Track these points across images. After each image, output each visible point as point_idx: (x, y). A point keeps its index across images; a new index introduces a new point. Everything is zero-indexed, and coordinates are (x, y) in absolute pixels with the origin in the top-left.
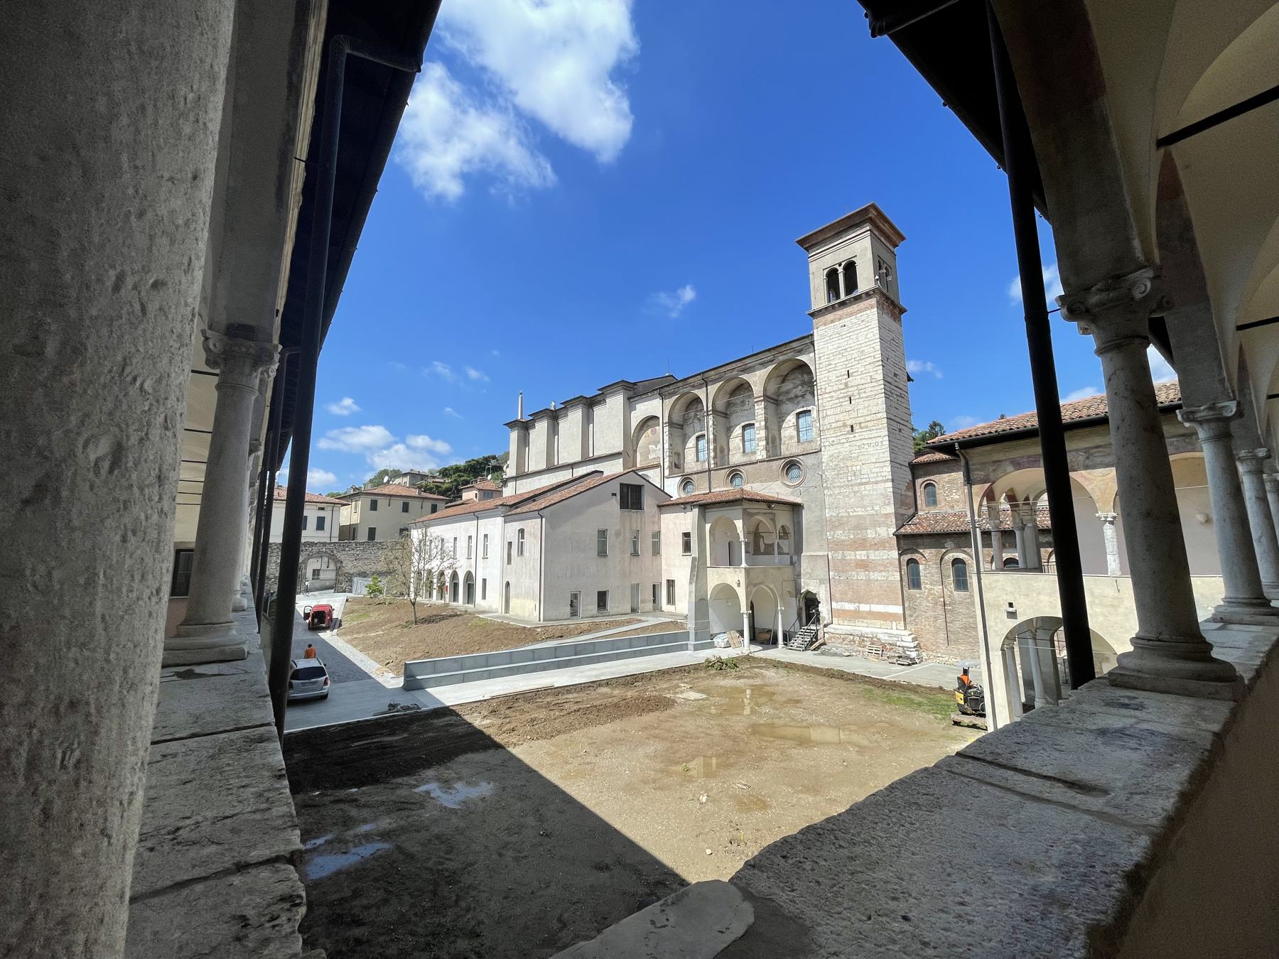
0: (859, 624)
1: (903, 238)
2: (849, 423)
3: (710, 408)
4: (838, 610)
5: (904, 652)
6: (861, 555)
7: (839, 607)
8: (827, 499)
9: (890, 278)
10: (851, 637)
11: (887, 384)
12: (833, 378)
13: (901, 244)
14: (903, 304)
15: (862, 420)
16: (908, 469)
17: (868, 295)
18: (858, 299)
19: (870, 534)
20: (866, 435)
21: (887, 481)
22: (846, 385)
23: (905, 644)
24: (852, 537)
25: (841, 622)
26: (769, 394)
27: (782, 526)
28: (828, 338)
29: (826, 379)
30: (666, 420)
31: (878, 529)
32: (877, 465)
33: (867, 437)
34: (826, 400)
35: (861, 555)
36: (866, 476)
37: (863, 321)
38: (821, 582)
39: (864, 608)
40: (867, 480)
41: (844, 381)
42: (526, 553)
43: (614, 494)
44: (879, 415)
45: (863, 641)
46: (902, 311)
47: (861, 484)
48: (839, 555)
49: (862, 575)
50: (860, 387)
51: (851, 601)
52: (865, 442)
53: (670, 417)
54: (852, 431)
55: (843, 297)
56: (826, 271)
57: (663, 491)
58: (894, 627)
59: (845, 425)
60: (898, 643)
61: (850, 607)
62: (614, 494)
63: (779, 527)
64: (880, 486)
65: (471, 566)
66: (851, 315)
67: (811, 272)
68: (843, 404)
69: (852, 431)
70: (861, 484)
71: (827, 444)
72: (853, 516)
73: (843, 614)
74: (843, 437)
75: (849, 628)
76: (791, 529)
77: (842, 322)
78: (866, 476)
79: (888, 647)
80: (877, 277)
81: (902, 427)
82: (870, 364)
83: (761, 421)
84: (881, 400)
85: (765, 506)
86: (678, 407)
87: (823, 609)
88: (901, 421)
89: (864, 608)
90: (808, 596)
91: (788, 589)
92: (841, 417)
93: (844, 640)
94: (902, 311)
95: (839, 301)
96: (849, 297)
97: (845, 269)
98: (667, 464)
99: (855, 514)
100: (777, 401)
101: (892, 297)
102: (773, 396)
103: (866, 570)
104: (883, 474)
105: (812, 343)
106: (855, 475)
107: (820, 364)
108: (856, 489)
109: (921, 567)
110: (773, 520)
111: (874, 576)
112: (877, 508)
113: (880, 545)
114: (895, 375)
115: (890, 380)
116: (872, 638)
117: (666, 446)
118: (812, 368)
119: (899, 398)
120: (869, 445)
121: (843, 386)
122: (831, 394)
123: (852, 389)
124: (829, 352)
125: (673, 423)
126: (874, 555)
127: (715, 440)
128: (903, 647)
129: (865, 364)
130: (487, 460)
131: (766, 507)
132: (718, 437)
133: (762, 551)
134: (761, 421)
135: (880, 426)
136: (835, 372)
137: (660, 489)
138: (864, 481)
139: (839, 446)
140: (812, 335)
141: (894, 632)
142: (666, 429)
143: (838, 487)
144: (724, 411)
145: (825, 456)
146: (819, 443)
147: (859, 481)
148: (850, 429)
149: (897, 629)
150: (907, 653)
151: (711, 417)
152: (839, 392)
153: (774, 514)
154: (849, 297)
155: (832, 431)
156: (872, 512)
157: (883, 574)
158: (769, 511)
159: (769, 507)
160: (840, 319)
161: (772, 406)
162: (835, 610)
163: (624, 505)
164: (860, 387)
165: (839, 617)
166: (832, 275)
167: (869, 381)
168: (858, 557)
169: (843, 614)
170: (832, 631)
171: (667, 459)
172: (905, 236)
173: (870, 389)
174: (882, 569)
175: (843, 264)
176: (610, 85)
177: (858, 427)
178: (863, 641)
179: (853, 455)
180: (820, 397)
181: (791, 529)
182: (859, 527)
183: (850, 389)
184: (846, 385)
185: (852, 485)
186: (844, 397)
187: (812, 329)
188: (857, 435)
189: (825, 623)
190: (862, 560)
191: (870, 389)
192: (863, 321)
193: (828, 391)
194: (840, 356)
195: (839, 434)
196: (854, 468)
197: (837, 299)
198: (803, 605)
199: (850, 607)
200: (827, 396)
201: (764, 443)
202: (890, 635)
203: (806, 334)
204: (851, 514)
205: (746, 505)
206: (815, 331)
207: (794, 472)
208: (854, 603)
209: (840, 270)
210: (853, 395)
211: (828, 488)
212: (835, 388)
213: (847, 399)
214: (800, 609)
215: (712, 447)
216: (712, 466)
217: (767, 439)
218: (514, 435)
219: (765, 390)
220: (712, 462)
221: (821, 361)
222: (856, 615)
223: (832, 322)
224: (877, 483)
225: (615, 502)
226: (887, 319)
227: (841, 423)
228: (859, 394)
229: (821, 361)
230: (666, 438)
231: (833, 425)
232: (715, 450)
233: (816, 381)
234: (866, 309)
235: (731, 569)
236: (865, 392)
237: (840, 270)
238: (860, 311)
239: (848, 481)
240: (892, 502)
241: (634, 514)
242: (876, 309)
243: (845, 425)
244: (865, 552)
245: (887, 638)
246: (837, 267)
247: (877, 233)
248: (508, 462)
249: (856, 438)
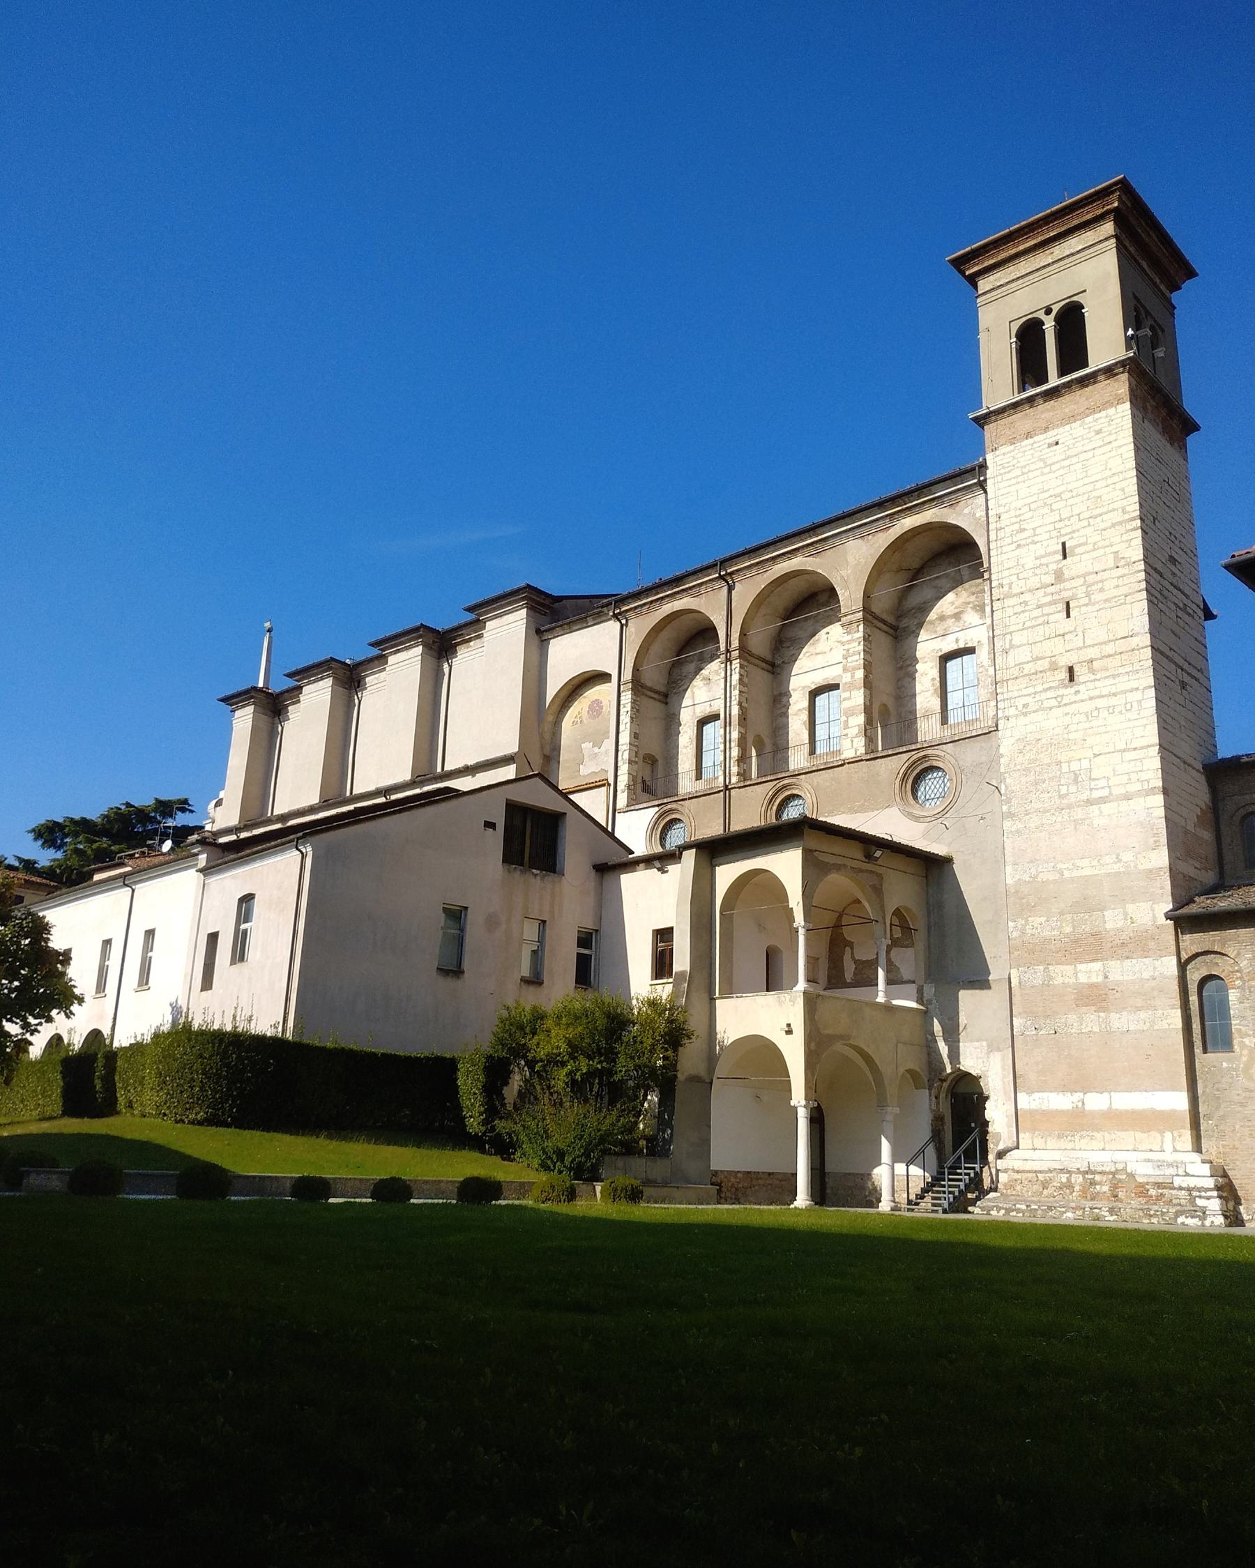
0: (1083, 1143)
1: (1191, 274)
2: (1065, 661)
3: (735, 643)
4: (1032, 1113)
5: (1192, 1200)
6: (1089, 972)
7: (1034, 1106)
8: (1008, 843)
9: (1160, 353)
10: (1064, 1178)
11: (1152, 572)
12: (1029, 562)
13: (1188, 285)
14: (1191, 405)
15: (1092, 653)
16: (1202, 779)
17: (1109, 371)
18: (1084, 382)
19: (1113, 920)
20: (1106, 686)
21: (1151, 791)
22: (1059, 576)
23: (1192, 1182)
24: (1068, 929)
25: (1039, 1143)
26: (876, 608)
27: (897, 913)
28: (1018, 472)
29: (1012, 563)
30: (627, 675)
31: (1130, 908)
32: (1129, 756)
33: (1105, 691)
34: (1010, 611)
35: (1089, 972)
36: (1102, 783)
37: (1098, 432)
38: (993, 1048)
39: (1096, 1102)
40: (1105, 793)
41: (1054, 566)
42: (254, 950)
43: (490, 825)
44: (1135, 641)
45: (1093, 1183)
46: (1190, 426)
47: (1090, 802)
48: (1036, 975)
49: (1091, 1021)
50: (1090, 579)
51: (1066, 1088)
52: (1101, 703)
53: (636, 669)
54: (1071, 679)
55: (1054, 380)
56: (1016, 327)
57: (611, 835)
58: (1168, 1146)
59: (1054, 667)
60: (1178, 1182)
61: (1061, 1102)
62: (490, 825)
63: (890, 910)
64: (1139, 804)
65: (101, 1017)
66: (1072, 418)
67: (982, 326)
68: (1052, 618)
69: (1071, 679)
70: (1090, 802)
71: (1012, 711)
72: (1072, 880)
73: (1047, 1122)
74: (1050, 694)
75: (1057, 1155)
76: (918, 922)
77: (1052, 435)
78: (1102, 783)
79: (1153, 1192)
80: (1130, 332)
81: (1187, 679)
82: (1113, 525)
83: (855, 669)
84: (1140, 606)
85: (855, 851)
86: (656, 648)
87: (997, 1114)
88: (1186, 666)
89: (1096, 1102)
90: (961, 1089)
91: (911, 1066)
92: (1047, 648)
93: (1045, 1185)
94: (1190, 426)
95: (1044, 387)
96: (1067, 379)
97: (1059, 319)
98: (623, 780)
99: (1076, 874)
100: (895, 628)
101: (1163, 381)
102: (884, 616)
103: (1105, 1010)
104: (1144, 776)
105: (982, 485)
106: (1076, 781)
107: (997, 530)
108: (1079, 813)
109: (1233, 995)
110: (878, 891)
111: (1121, 1021)
112: (1127, 857)
113: (1133, 945)
114: (1173, 560)
115: (1159, 566)
116: (1114, 1174)
117: (625, 738)
118: (983, 549)
119: (1180, 613)
120: (1111, 710)
121: (1050, 579)
122: (1023, 598)
123: (1074, 583)
124: (1019, 504)
125: (643, 686)
126: (1122, 971)
127: (743, 719)
128: (1189, 1189)
129: (1103, 526)
130: (166, 808)
131: (860, 856)
132: (751, 714)
133: (849, 976)
134: (855, 669)
135: (1136, 666)
136: (1032, 547)
137: (605, 830)
138: (1096, 794)
139: (1038, 716)
140: (983, 466)
141: (1169, 1156)
142: (627, 697)
143: (1038, 811)
144: (769, 657)
145: (1007, 741)
146: (992, 713)
147: (1084, 797)
148: (1065, 675)
149: (1175, 1150)
150: (1200, 1202)
151: (736, 664)
152: (1041, 592)
153: (880, 876)
154: (1067, 379)
155: (1023, 682)
156: (1117, 867)
157: (1143, 1015)
158: (869, 867)
159: (869, 857)
160: (1046, 429)
161: (883, 640)
162: (1025, 1111)
163: (512, 856)
164: (1090, 579)
165: (1033, 1130)
166: (1029, 335)
167: (1111, 564)
168: (1083, 979)
169: (1047, 1122)
170: (1018, 1165)
171: (624, 769)
172: (1196, 266)
173: (1115, 582)
174: (1139, 1003)
175: (1056, 309)
176: (511, 1084)
177: (1085, 670)
178: (1093, 1183)
179: (1072, 736)
180: (996, 605)
181: (918, 922)
182: (1086, 905)
183: (1067, 585)
184: (1059, 576)
185: (1070, 807)
186: (1054, 603)
187: (982, 451)
188: (1081, 688)
189: (1001, 1147)
190: (1092, 986)
191: (1115, 582)
192: (1098, 432)
193: (1016, 590)
194: (1046, 510)
195: (1039, 688)
196: (1075, 766)
197: (1039, 384)
198: (946, 1109)
199: (1061, 1102)
200: (1014, 601)
201: (861, 719)
202: (1160, 1164)
203: (968, 466)
204: (1067, 874)
205: (813, 840)
206: (989, 457)
207: (930, 785)
208: (1073, 1091)
209: (1049, 324)
210: (1074, 597)
211: (1011, 815)
212: (1034, 582)
213: (1062, 606)
214: (938, 1120)
215: (735, 735)
216: (734, 779)
217: (868, 710)
218: (244, 719)
219: (867, 596)
220: (735, 769)
221: (1002, 524)
222: (1077, 1122)
223: (1029, 435)
224: (1128, 797)
225: (496, 840)
226: (1155, 436)
227: (1045, 664)
228: (1088, 595)
229: (1002, 524)
230: (625, 719)
231: (1028, 668)
232: (742, 742)
233: (989, 569)
234: (1106, 405)
235: (771, 997)
236: (1102, 590)
237: (1049, 324)
238: (1093, 410)
239: (1061, 797)
240: (1164, 840)
241: (536, 882)
242: (1128, 405)
243: (1054, 667)
244: (1097, 966)
245: (1151, 1171)
246: (1041, 315)
247: (1132, 249)
248: (222, 795)
249: (1080, 697)
